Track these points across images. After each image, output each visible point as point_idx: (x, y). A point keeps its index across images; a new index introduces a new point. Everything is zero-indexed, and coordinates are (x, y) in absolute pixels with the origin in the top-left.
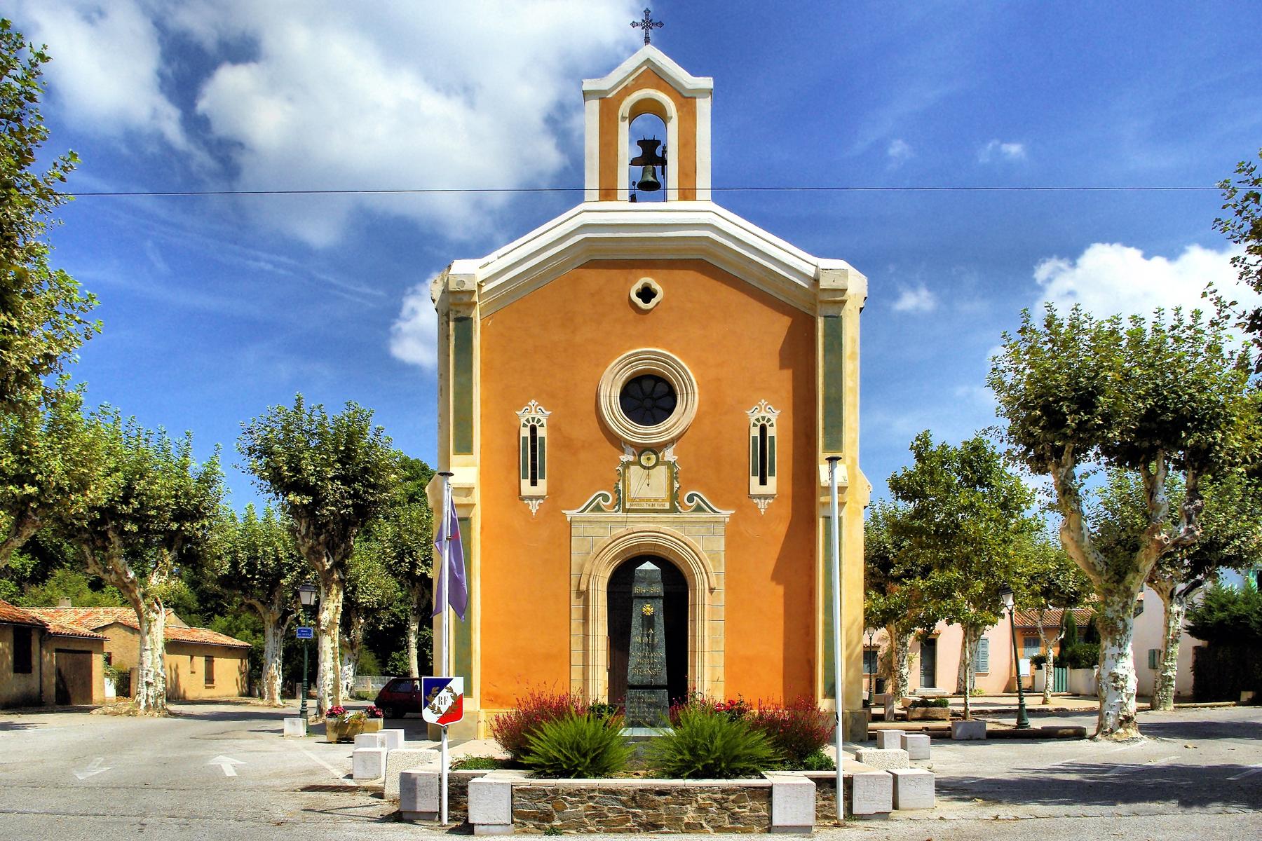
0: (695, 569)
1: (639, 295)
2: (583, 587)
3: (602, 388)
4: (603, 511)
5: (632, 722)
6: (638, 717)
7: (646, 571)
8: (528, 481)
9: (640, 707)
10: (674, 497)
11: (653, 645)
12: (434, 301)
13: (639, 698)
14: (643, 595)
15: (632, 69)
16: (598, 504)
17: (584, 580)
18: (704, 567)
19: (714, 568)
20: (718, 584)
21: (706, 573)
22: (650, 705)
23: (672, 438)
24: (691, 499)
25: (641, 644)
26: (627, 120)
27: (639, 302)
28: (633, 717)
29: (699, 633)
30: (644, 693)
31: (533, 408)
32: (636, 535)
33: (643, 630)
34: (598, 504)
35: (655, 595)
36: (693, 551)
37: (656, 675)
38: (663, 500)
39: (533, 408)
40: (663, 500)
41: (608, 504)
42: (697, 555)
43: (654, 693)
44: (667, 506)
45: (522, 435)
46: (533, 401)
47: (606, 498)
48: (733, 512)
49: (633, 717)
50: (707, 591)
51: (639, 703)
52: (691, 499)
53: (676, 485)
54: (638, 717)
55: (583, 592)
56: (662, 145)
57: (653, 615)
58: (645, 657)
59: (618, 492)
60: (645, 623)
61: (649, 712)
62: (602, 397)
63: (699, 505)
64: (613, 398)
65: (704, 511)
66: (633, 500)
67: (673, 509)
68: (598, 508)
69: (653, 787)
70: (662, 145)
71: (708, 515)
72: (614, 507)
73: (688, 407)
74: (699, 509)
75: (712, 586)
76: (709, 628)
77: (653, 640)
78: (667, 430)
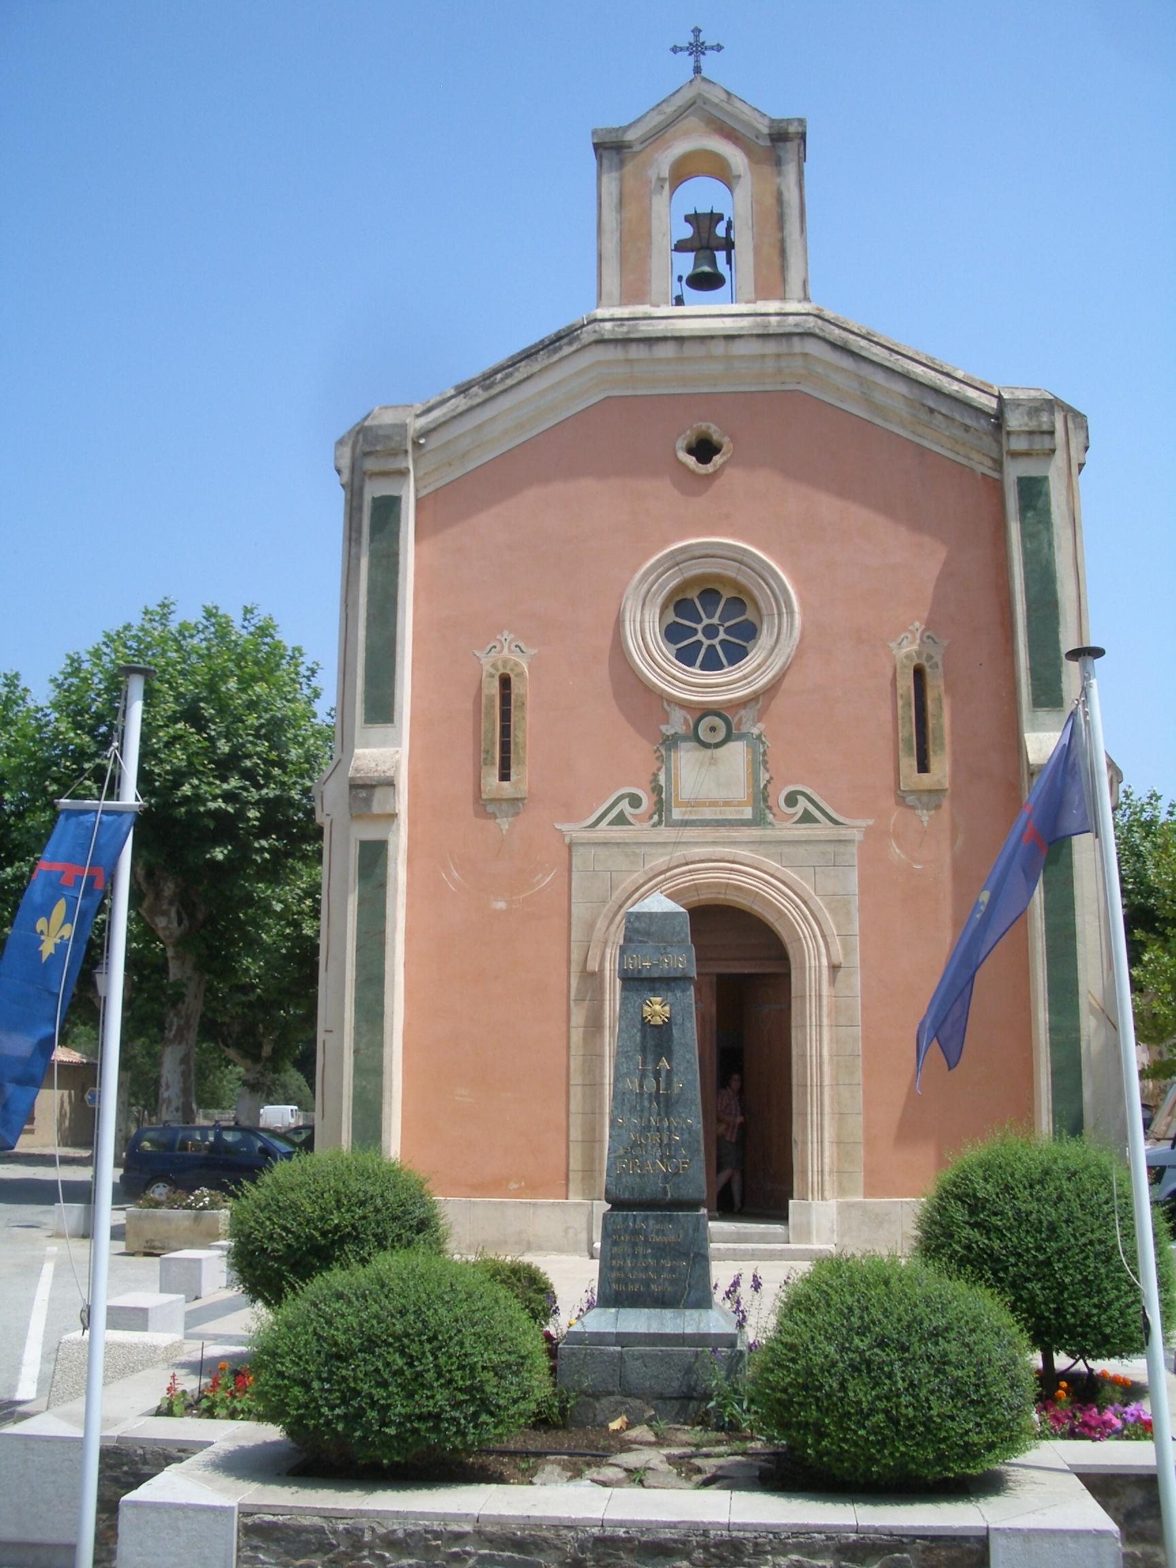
0: (803, 930)
1: (690, 451)
2: (593, 966)
3: (628, 608)
4: (630, 824)
5: (617, 1293)
6: (633, 1282)
7: (651, 916)
8: (496, 771)
9: (635, 1256)
10: (761, 798)
11: (668, 1098)
12: (339, 471)
13: (635, 1232)
14: (645, 974)
15: (892, 774)
16: (622, 812)
17: (594, 953)
18: (819, 924)
19: (838, 927)
20: (846, 955)
21: (824, 936)
22: (662, 1250)
23: (755, 692)
24: (791, 800)
25: (641, 1094)
26: (667, 186)
27: (691, 461)
28: (618, 1281)
29: (812, 1051)
30: (646, 1219)
31: (506, 646)
32: (691, 867)
33: (644, 1063)
34: (622, 812)
35: (672, 975)
36: (765, 872)
37: (676, 1174)
38: (740, 804)
39: (506, 646)
40: (740, 804)
41: (637, 811)
42: (805, 902)
43: (671, 1219)
44: (748, 813)
45: (485, 691)
46: (506, 634)
47: (635, 801)
48: (871, 822)
49: (618, 1281)
50: (825, 972)
51: (634, 1245)
52: (791, 800)
53: (764, 777)
54: (633, 1282)
55: (593, 974)
56: (726, 219)
57: (667, 1026)
58: (648, 1127)
59: (657, 789)
60: (651, 1043)
61: (659, 1270)
62: (627, 623)
63: (806, 812)
64: (647, 625)
65: (816, 821)
66: (688, 804)
67: (758, 821)
68: (621, 820)
69: (633, 1532)
70: (726, 219)
71: (822, 830)
72: (651, 817)
73: (783, 637)
74: (807, 818)
75: (835, 961)
76: (831, 1040)
77: (669, 1084)
78: (745, 677)
